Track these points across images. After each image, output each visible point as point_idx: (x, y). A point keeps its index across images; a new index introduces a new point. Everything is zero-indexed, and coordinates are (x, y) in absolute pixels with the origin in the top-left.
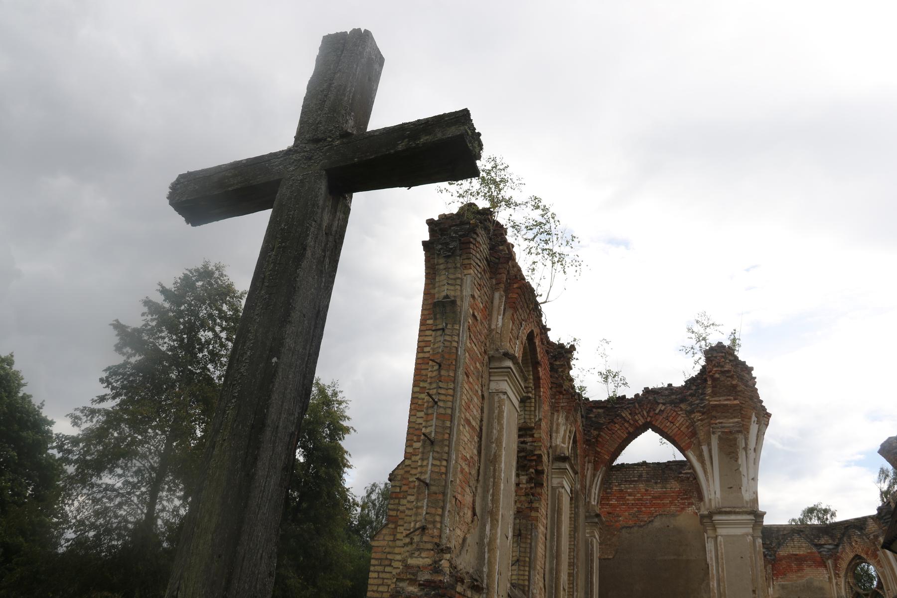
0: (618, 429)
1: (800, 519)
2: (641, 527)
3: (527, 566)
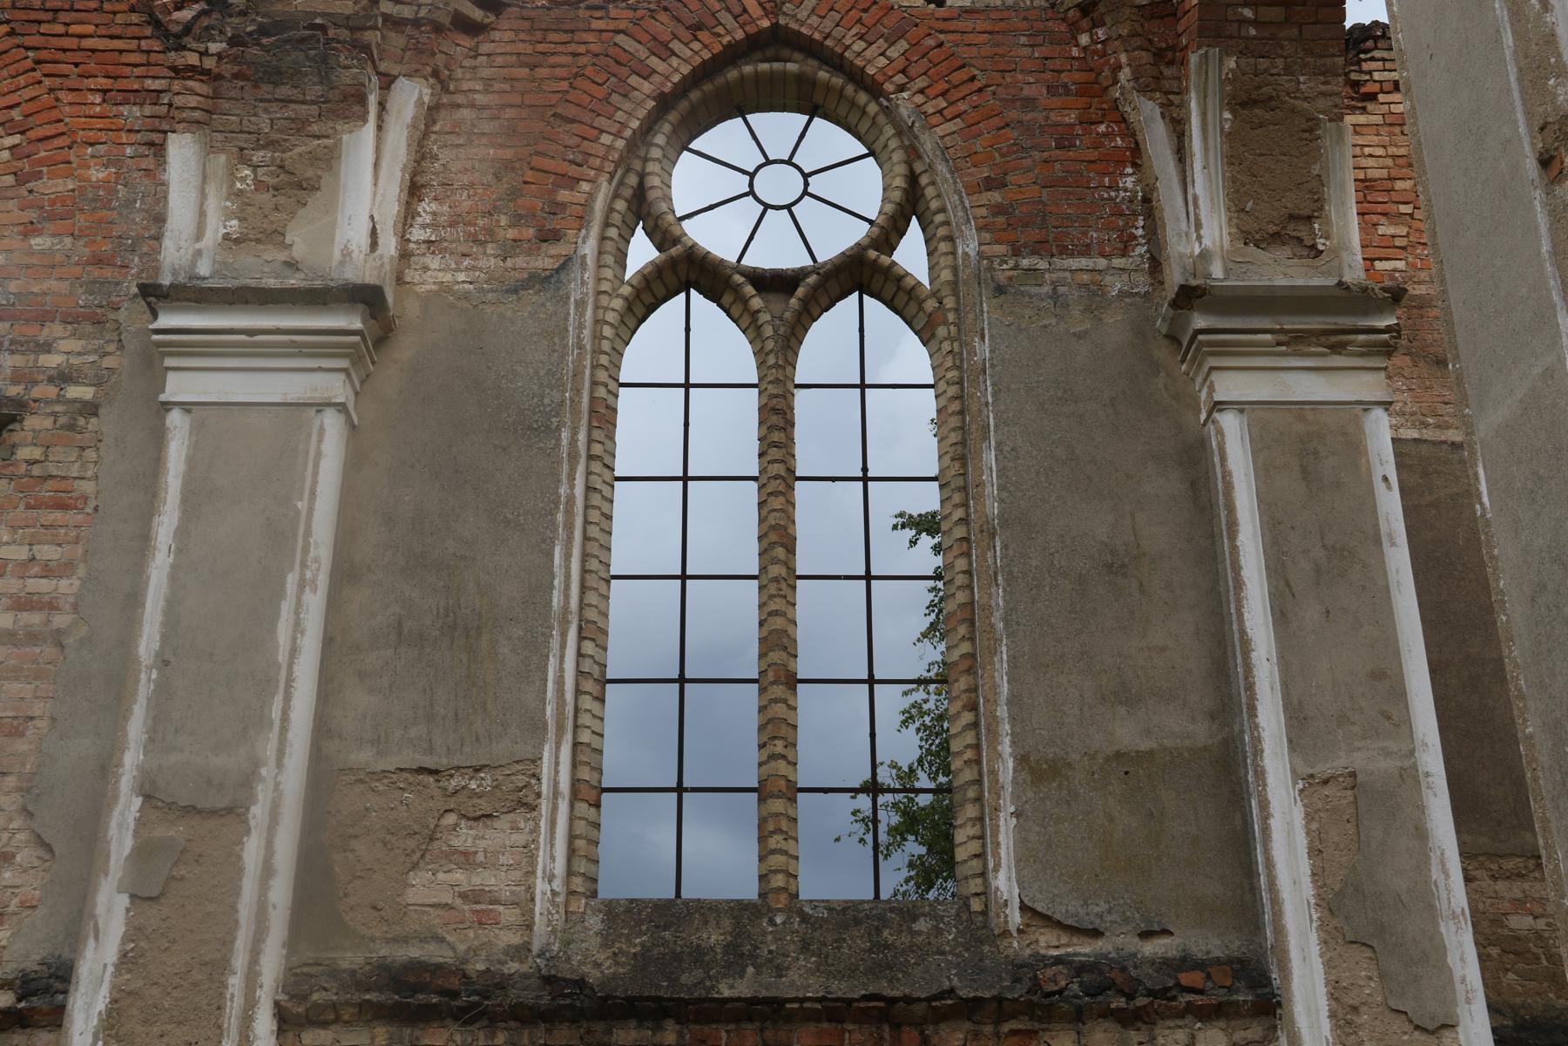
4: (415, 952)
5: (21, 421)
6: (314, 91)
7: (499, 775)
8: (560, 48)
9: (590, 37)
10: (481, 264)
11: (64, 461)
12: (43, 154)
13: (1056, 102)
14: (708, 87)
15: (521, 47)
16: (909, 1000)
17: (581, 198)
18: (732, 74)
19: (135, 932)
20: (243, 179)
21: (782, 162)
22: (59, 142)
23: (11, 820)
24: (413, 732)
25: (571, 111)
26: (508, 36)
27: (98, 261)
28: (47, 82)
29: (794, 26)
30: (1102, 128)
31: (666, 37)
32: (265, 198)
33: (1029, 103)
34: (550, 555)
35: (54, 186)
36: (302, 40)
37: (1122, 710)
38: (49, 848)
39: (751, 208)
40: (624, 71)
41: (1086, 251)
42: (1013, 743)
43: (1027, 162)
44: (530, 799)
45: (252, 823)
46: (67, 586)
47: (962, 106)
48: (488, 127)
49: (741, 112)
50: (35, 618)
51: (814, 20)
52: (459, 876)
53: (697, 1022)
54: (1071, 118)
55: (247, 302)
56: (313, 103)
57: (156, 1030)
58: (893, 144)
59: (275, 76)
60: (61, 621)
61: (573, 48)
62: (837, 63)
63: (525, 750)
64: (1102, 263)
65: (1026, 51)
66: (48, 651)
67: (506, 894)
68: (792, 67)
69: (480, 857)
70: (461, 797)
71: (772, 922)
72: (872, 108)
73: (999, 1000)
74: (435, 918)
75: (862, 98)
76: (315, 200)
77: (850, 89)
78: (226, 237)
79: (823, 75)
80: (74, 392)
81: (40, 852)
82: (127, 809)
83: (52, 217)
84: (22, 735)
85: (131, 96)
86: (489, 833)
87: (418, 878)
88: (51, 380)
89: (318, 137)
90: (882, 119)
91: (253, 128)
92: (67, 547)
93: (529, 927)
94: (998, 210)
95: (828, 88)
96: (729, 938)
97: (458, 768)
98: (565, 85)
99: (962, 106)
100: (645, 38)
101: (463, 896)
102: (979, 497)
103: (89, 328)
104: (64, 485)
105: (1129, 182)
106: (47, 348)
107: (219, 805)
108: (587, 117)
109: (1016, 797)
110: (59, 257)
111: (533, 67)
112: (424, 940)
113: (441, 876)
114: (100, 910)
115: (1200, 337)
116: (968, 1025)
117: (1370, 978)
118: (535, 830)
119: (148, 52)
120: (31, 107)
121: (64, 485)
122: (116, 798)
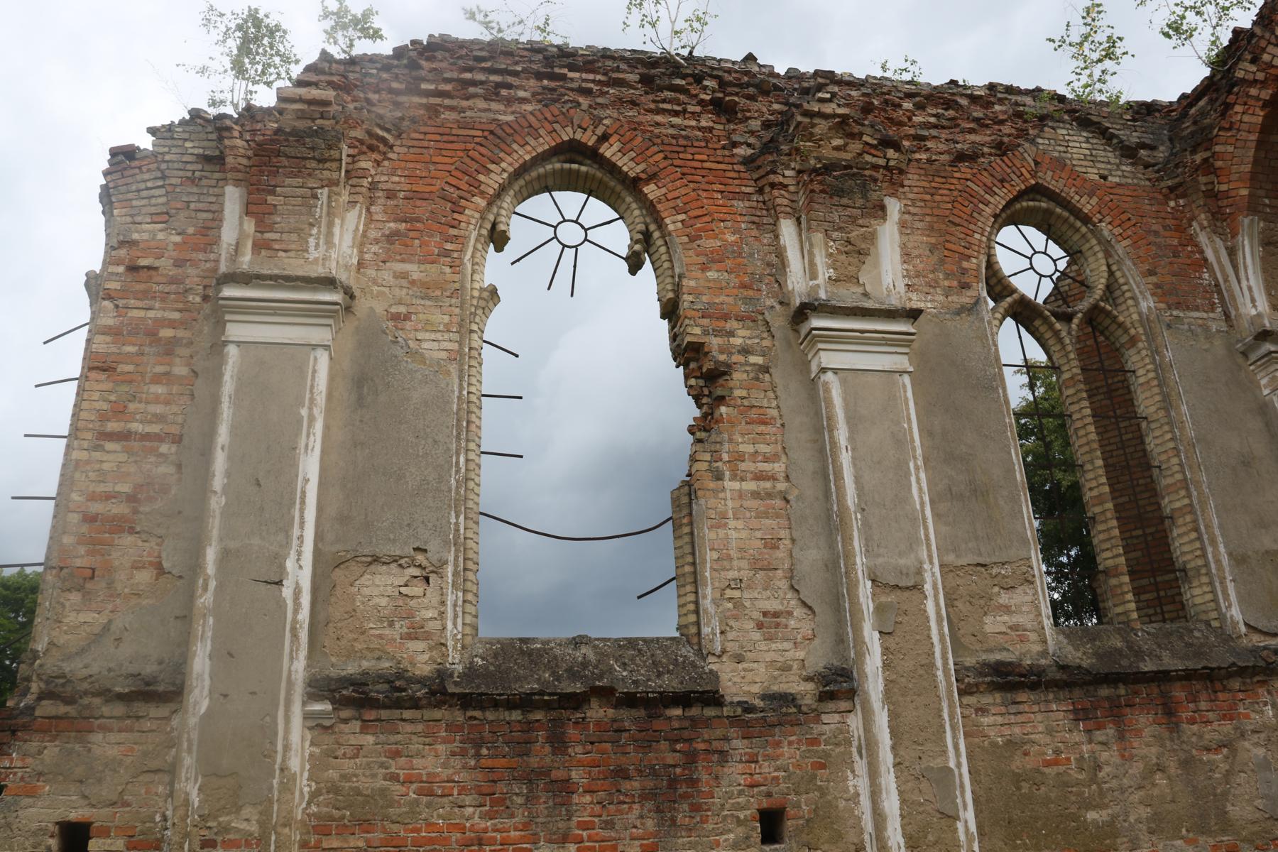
0: (1243, 113)
1: (354, 16)
2: (167, 213)
3: (1122, 574)
4: (998, 656)
5: (730, 375)
6: (859, 202)
7: (1014, 566)
8: (942, 186)
9: (955, 181)
10: (936, 298)
11: (758, 398)
12: (699, 225)
13: (1168, 234)
14: (1009, 212)
15: (924, 184)
16: (1219, 668)
17: (974, 267)
18: (1018, 206)
19: (886, 650)
20: (831, 247)
21: (572, 221)
22: (707, 219)
23: (785, 594)
24: (970, 545)
25: (957, 220)
26: (916, 177)
27: (744, 286)
28: (691, 185)
29: (1046, 185)
30: (1189, 248)
31: (991, 185)
32: (843, 257)
33: (1156, 233)
34: (1010, 453)
35: (710, 244)
36: (854, 175)
37: (1263, 531)
38: (810, 608)
39: (555, 247)
40: (975, 201)
41: (1197, 309)
42: (1225, 547)
43: (1163, 263)
44: (1030, 578)
45: (927, 593)
46: (778, 467)
47: (1129, 232)
48: (920, 225)
49: (548, 189)
50: (768, 485)
51: (1053, 182)
52: (1006, 618)
53: (1132, 684)
54: (1175, 242)
55: (855, 315)
56: (859, 208)
57: (908, 699)
58: (1097, 248)
59: (840, 193)
60: (782, 486)
61: (947, 186)
62: (1066, 204)
63: (1023, 554)
64: (1205, 315)
65: (1148, 207)
66: (779, 503)
67: (1029, 626)
68: (1044, 205)
69: (1013, 608)
70: (999, 578)
71: (1136, 635)
72: (1084, 229)
73: (1254, 667)
74: (1000, 638)
75: (1078, 224)
76: (869, 260)
77: (1072, 219)
78: (830, 278)
79: (1058, 210)
80: (753, 359)
81: (805, 610)
82: (865, 589)
83: (713, 261)
84: (778, 548)
85: (737, 196)
86: (1015, 596)
87: (988, 619)
88: (739, 352)
89: (862, 227)
90: (1089, 235)
91: (831, 220)
92: (772, 446)
93: (1045, 642)
94: (1157, 286)
95: (1059, 216)
96: (492, 668)
97: (995, 563)
98: (949, 206)
99: (1129, 232)
100: (981, 184)
101: (1010, 628)
102: (1182, 429)
103: (751, 324)
104: (761, 411)
105: (1206, 276)
106: (731, 334)
107: (910, 584)
108: (965, 224)
109: (1232, 573)
110: (724, 284)
111: (932, 195)
112: (1000, 650)
113: (998, 618)
114: (867, 640)
115: (814, 332)
116: (1240, 679)
117: (682, 683)
118: (1036, 593)
119: (739, 172)
120: (685, 199)
121: (761, 411)
122: (858, 581)
